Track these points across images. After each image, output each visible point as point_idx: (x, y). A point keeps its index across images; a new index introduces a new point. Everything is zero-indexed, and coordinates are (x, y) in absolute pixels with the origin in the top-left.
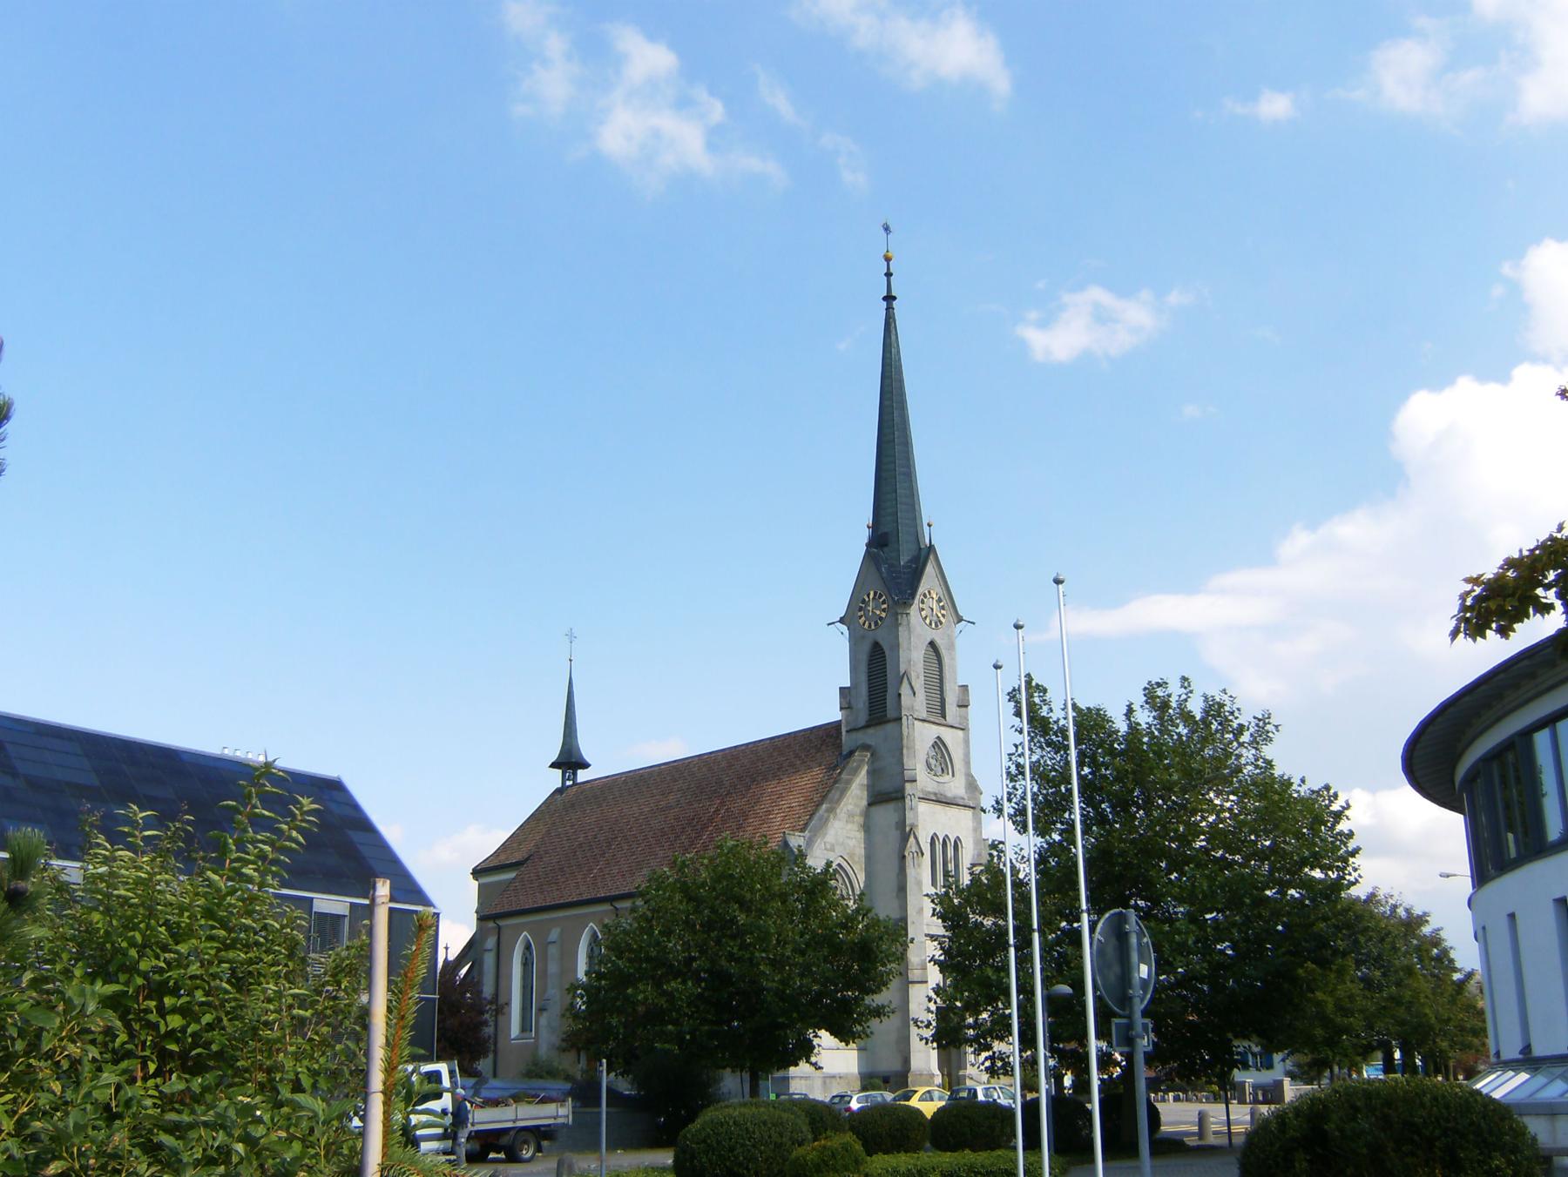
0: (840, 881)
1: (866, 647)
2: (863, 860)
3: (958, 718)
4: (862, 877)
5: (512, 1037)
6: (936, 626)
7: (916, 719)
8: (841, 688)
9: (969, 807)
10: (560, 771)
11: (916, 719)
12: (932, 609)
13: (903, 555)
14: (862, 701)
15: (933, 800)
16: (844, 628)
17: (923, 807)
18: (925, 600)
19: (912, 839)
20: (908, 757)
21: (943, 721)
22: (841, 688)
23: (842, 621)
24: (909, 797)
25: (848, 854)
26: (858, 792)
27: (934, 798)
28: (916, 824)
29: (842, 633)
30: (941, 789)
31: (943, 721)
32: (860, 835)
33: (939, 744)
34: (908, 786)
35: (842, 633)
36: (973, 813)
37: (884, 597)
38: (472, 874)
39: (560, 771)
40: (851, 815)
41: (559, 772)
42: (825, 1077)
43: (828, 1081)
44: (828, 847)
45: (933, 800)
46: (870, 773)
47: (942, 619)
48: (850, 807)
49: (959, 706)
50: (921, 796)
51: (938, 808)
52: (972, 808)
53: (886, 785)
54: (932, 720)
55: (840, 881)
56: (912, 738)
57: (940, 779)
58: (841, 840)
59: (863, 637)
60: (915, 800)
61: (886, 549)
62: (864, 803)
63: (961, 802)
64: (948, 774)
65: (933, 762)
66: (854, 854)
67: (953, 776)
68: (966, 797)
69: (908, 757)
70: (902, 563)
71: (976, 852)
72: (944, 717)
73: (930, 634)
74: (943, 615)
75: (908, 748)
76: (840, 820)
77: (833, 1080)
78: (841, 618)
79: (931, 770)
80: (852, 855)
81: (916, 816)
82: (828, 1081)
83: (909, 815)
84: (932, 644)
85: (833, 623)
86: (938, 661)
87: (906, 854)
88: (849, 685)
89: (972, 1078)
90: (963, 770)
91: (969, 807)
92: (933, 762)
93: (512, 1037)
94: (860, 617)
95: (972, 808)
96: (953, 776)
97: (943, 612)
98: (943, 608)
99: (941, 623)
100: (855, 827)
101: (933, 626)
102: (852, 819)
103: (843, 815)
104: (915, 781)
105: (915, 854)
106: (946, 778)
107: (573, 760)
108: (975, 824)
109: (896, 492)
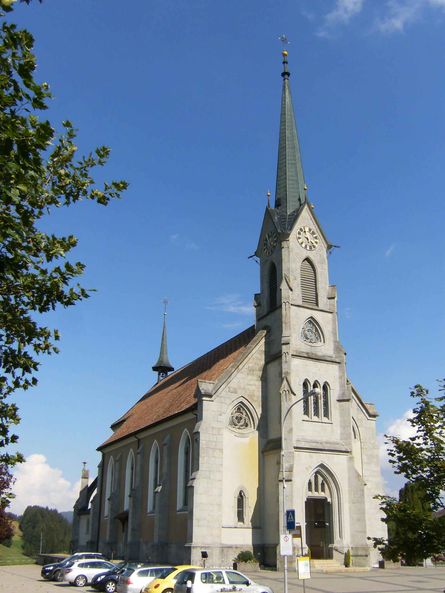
0: (244, 412)
1: (268, 266)
2: (260, 399)
3: (329, 306)
4: (259, 411)
5: (148, 512)
6: (310, 248)
7: (292, 305)
8: (255, 294)
9: (336, 362)
10: (158, 372)
11: (292, 305)
12: (307, 238)
13: (289, 209)
14: (265, 301)
15: (305, 357)
16: (258, 259)
17: (296, 362)
18: (302, 233)
19: (285, 382)
20: (285, 329)
21: (316, 308)
22: (255, 294)
23: (256, 254)
24: (284, 354)
25: (248, 395)
26: (258, 356)
27: (306, 356)
28: (289, 372)
29: (256, 261)
30: (313, 350)
31: (316, 308)
32: (259, 383)
33: (312, 321)
34: (284, 347)
35: (256, 261)
36: (339, 366)
37: (275, 234)
38: (111, 427)
39: (158, 372)
40: (251, 371)
41: (157, 373)
42: (222, 547)
43: (225, 550)
44: (232, 390)
45: (305, 357)
46: (266, 343)
47: (315, 244)
48: (250, 365)
49: (329, 298)
50: (295, 354)
51: (310, 363)
52: (339, 363)
53: (274, 351)
54: (306, 306)
55: (245, 414)
56: (288, 316)
57: (315, 345)
58: (243, 386)
59: (266, 261)
60: (289, 357)
61: (280, 208)
62: (263, 362)
63: (328, 359)
64: (321, 342)
65: (309, 334)
66: (254, 396)
67: (324, 343)
68: (334, 356)
69: (285, 329)
70: (288, 214)
71: (341, 392)
72: (317, 305)
73: (306, 254)
74: (316, 243)
75: (286, 323)
76: (242, 373)
77: (230, 549)
78: (255, 253)
79: (308, 339)
80: (252, 396)
81: (289, 367)
82: (225, 550)
83: (284, 366)
84: (307, 259)
85: (252, 257)
86: (312, 268)
87: (281, 392)
88: (260, 293)
89: (337, 550)
90: (332, 339)
91: (336, 362)
92: (309, 334)
93: (148, 512)
94: (264, 250)
95: (339, 363)
96: (324, 343)
97: (315, 240)
98: (316, 238)
99: (314, 247)
100: (255, 378)
101: (308, 248)
102: (252, 372)
103: (244, 369)
104: (289, 343)
105: (287, 392)
106: (319, 344)
107: (162, 365)
108: (340, 374)
109: (286, 174)
